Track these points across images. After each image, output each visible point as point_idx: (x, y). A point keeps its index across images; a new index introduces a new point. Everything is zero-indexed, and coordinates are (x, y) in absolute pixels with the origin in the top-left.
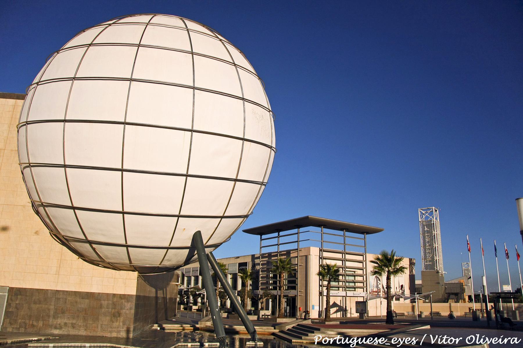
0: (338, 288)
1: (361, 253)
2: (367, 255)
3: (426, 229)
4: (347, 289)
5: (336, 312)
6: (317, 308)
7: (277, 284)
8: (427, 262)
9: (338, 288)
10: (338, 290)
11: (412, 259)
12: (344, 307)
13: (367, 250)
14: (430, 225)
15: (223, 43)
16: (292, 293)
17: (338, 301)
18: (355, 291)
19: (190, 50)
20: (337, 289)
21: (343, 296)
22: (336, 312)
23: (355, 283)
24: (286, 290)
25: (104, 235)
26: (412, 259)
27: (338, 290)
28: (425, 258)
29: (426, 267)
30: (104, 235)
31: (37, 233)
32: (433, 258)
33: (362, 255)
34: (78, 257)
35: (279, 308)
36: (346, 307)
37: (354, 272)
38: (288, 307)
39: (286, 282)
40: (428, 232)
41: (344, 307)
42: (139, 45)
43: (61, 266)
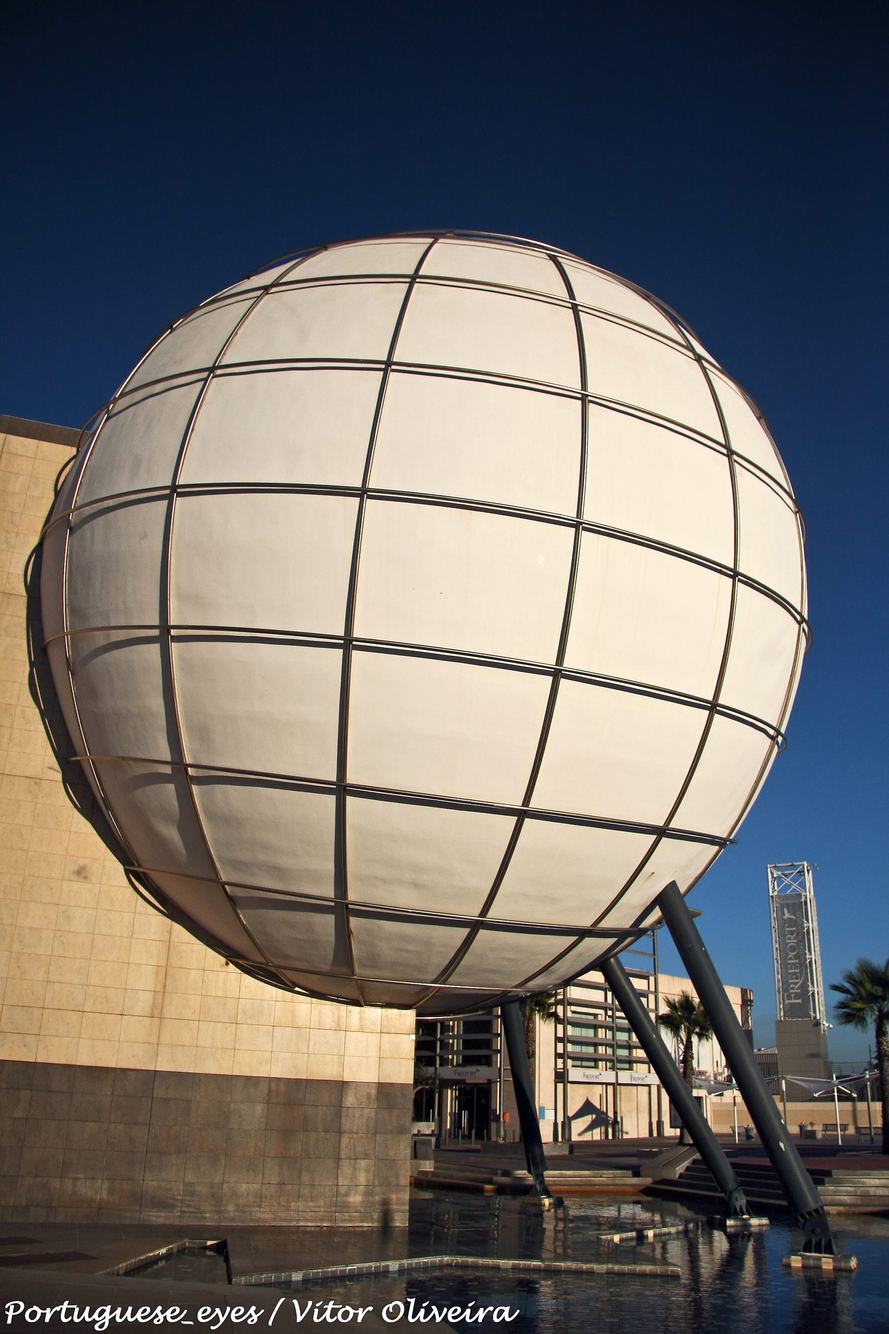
0: (596, 1061)
1: (644, 971)
2: (662, 978)
3: (787, 915)
4: (619, 1065)
5: (590, 1128)
6: (549, 1115)
7: (435, 1049)
8: (789, 998)
9: (596, 1061)
10: (596, 1067)
11: (746, 990)
12: (611, 1114)
13: (659, 963)
14: (797, 906)
15: (704, 370)
16: (477, 1075)
17: (595, 1095)
18: (631, 1069)
19: (578, 386)
20: (592, 1064)
21: (607, 1084)
22: (590, 1128)
23: (596, 1045)
24: (458, 1065)
25: (416, 885)
26: (746, 990)
27: (596, 1067)
28: (786, 988)
29: (791, 1011)
30: (416, 885)
31: (81, 873)
32: (804, 988)
33: (646, 978)
34: (223, 960)
35: (650, 1124)
36: (615, 1113)
37: (595, 1015)
38: (465, 1115)
39: (456, 1044)
40: (790, 922)
41: (611, 1114)
42: (388, 366)
43: (169, 988)
